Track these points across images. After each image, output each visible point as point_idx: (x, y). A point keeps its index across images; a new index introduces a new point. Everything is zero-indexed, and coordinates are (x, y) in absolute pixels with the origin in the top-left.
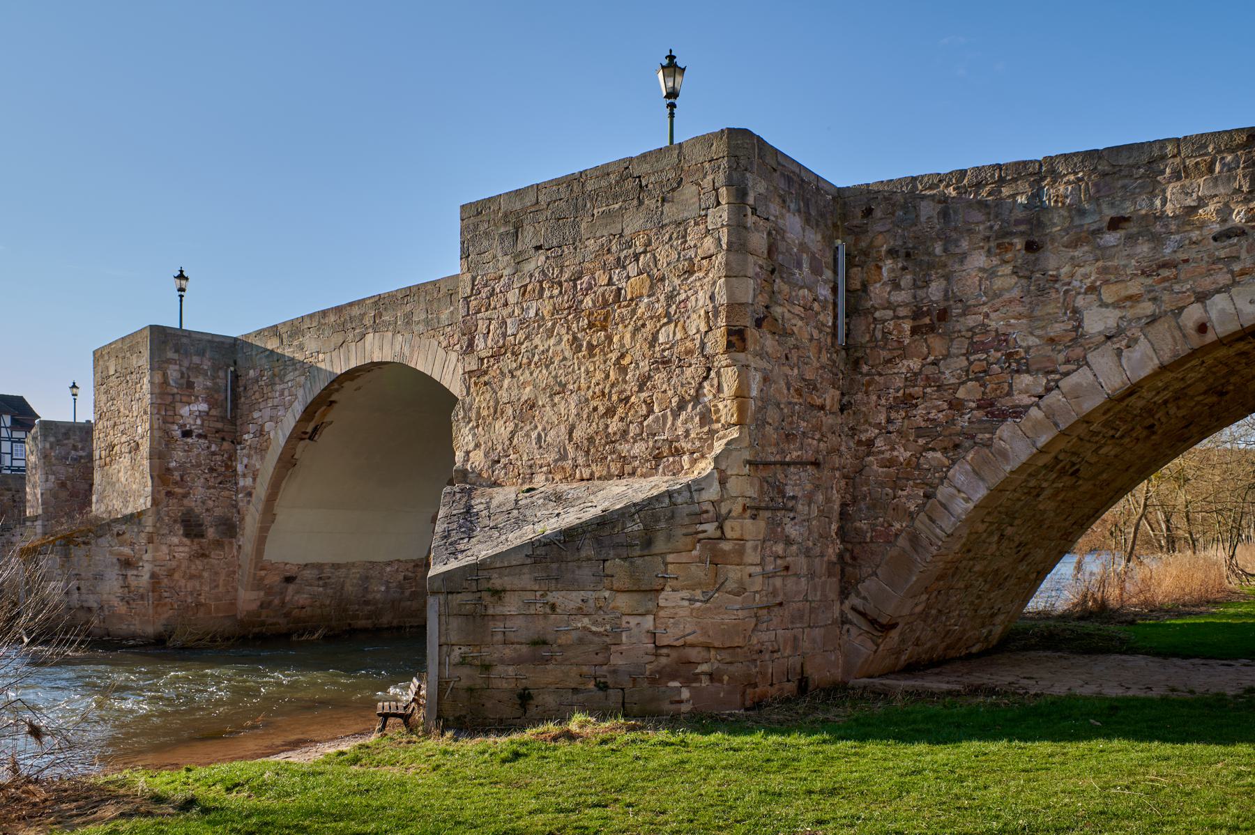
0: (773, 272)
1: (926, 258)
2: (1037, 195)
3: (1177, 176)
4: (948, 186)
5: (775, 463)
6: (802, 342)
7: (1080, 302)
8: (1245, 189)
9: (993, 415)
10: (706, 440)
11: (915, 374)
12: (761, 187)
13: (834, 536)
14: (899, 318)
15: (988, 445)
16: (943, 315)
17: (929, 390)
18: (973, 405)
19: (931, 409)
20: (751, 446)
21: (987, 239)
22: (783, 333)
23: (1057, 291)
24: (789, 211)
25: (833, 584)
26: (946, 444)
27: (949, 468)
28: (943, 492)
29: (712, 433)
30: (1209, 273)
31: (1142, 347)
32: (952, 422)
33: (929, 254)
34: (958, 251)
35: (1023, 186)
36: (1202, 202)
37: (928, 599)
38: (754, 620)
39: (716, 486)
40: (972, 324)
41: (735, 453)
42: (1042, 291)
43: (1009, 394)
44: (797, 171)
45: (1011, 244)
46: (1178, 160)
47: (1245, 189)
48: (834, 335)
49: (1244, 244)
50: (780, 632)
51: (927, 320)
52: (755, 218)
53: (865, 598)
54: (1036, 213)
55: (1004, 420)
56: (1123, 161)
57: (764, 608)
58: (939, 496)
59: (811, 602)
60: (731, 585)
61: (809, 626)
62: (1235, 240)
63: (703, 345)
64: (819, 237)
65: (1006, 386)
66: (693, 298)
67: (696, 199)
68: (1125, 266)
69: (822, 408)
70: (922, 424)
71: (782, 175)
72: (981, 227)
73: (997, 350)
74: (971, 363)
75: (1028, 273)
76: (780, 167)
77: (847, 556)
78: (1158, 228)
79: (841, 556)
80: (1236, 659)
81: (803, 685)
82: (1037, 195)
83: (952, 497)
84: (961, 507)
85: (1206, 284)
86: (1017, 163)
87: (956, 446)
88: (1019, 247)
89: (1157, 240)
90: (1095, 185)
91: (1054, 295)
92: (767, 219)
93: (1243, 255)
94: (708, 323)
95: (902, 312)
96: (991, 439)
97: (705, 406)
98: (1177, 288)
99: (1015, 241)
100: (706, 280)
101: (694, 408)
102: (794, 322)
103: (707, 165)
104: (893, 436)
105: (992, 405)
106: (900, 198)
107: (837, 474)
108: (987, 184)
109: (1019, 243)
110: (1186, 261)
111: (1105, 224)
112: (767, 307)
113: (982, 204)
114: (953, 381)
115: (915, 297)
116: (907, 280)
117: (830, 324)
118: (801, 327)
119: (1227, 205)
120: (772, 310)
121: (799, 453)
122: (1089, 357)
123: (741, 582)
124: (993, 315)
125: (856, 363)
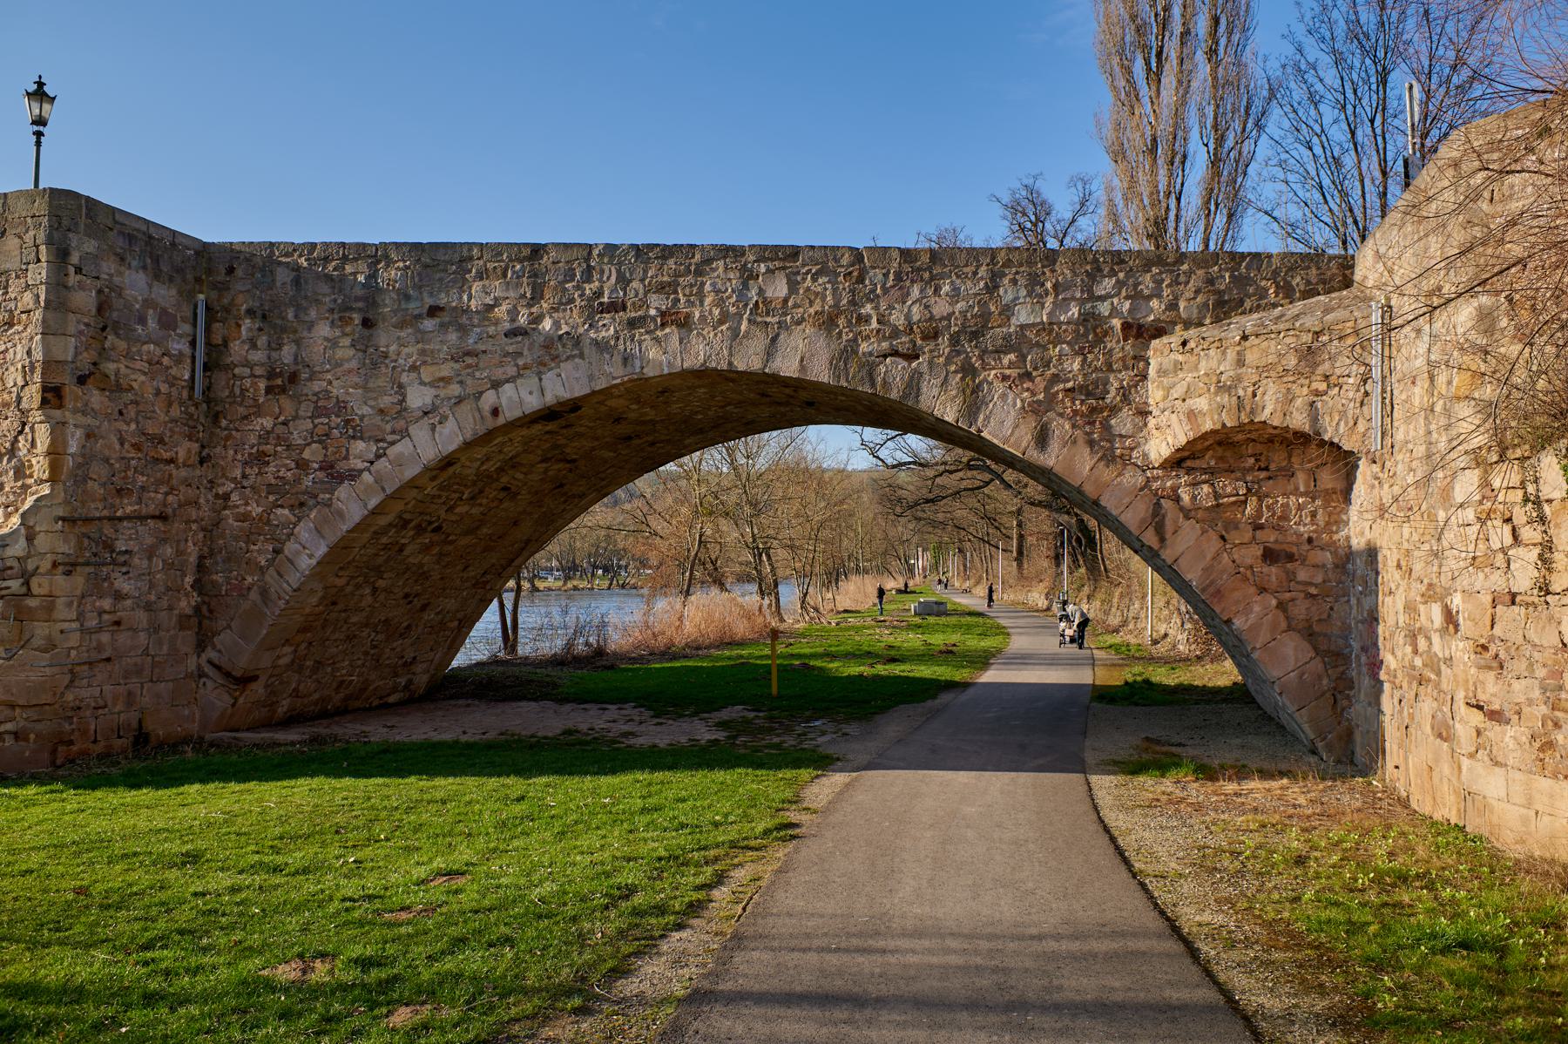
0: (104, 329)
1: (279, 322)
2: (373, 276)
3: (480, 277)
4: (300, 256)
5: (100, 519)
6: (143, 397)
7: (404, 378)
8: (528, 295)
9: (333, 478)
10: (20, 495)
11: (268, 433)
12: (90, 246)
13: (189, 589)
14: (255, 377)
15: (328, 504)
16: (293, 378)
17: (279, 449)
18: (316, 466)
19: (280, 468)
20: (67, 502)
21: (332, 311)
22: (115, 387)
23: (387, 366)
24: (130, 267)
25: (190, 636)
26: (292, 502)
27: (295, 525)
28: (290, 547)
29: (25, 487)
30: (501, 364)
31: (451, 424)
32: (298, 481)
33: (283, 319)
34: (307, 318)
35: (362, 266)
36: (497, 302)
37: (296, 651)
38: (67, 678)
39: (22, 542)
40: (317, 389)
41: (44, 510)
42: (375, 365)
43: (346, 458)
44: (144, 228)
45: (351, 318)
46: (481, 262)
47: (528, 295)
48: (192, 388)
49: (527, 342)
50: (107, 688)
51: (279, 382)
52: (79, 277)
53: (220, 651)
54: (372, 293)
55: (342, 482)
56: (441, 256)
57: (84, 663)
58: (286, 552)
59: (153, 657)
60: (37, 642)
61: (151, 681)
62: (520, 338)
63: (19, 399)
64: (173, 292)
65: (344, 450)
66: (11, 351)
67: (17, 252)
68: (439, 351)
69: (171, 461)
70: (273, 481)
71: (121, 233)
72: (327, 299)
73: (337, 416)
74: (315, 426)
75: (363, 348)
76: (118, 226)
77: (204, 609)
78: (464, 320)
79: (197, 609)
80: (626, 702)
81: (141, 738)
82: (373, 276)
83: (298, 553)
84: (306, 563)
85: (499, 374)
86: (358, 245)
87: (302, 504)
88: (356, 322)
89: (463, 330)
90: (419, 274)
91: (383, 370)
92: (98, 278)
93: (526, 352)
94: (24, 377)
95: (259, 371)
96: (330, 499)
97: (20, 460)
98: (477, 374)
99: (355, 316)
100: (24, 335)
101: (9, 461)
102: (133, 377)
103: (29, 220)
104: (248, 491)
105: (332, 467)
106: (258, 260)
107: (194, 527)
108: (333, 260)
109: (357, 318)
110: (484, 352)
111: (425, 311)
112: (95, 364)
113: (328, 278)
114: (300, 442)
115: (269, 358)
116: (262, 341)
117: (186, 377)
118: (143, 382)
119: (515, 307)
120: (101, 367)
121: (136, 507)
122: (411, 429)
123: (49, 638)
124: (335, 383)
125: (216, 418)
